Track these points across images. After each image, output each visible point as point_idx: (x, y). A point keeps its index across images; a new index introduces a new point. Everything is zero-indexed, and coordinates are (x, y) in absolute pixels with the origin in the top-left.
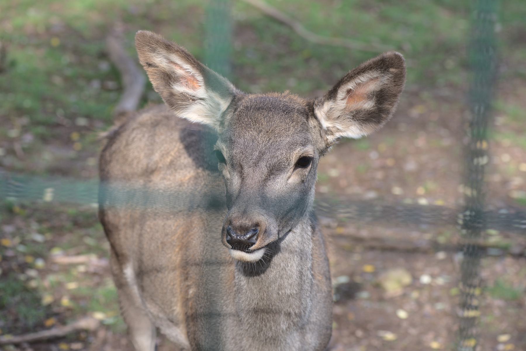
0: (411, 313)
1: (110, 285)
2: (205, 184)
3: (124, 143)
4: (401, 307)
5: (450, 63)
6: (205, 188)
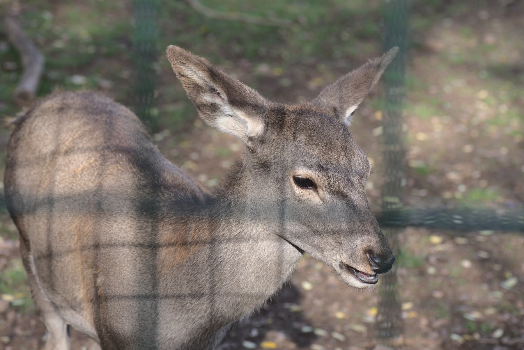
0: (315, 284)
1: (18, 266)
2: (98, 174)
3: (28, 130)
4: (306, 279)
5: (346, 35)
6: (99, 178)
